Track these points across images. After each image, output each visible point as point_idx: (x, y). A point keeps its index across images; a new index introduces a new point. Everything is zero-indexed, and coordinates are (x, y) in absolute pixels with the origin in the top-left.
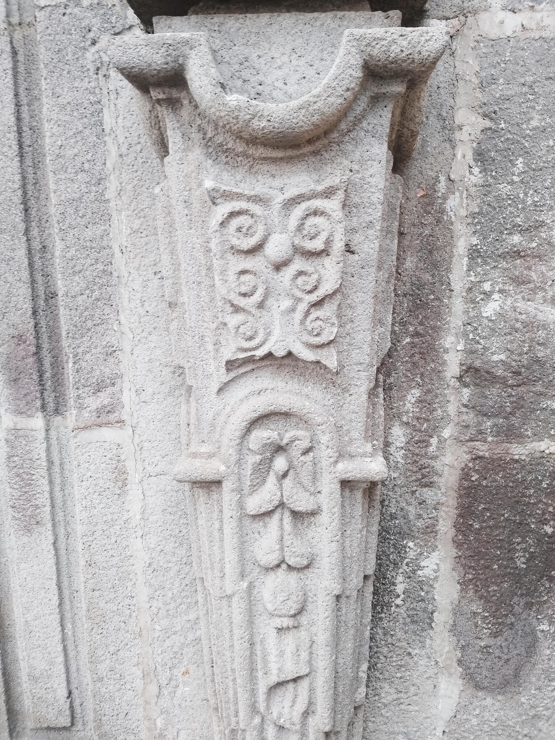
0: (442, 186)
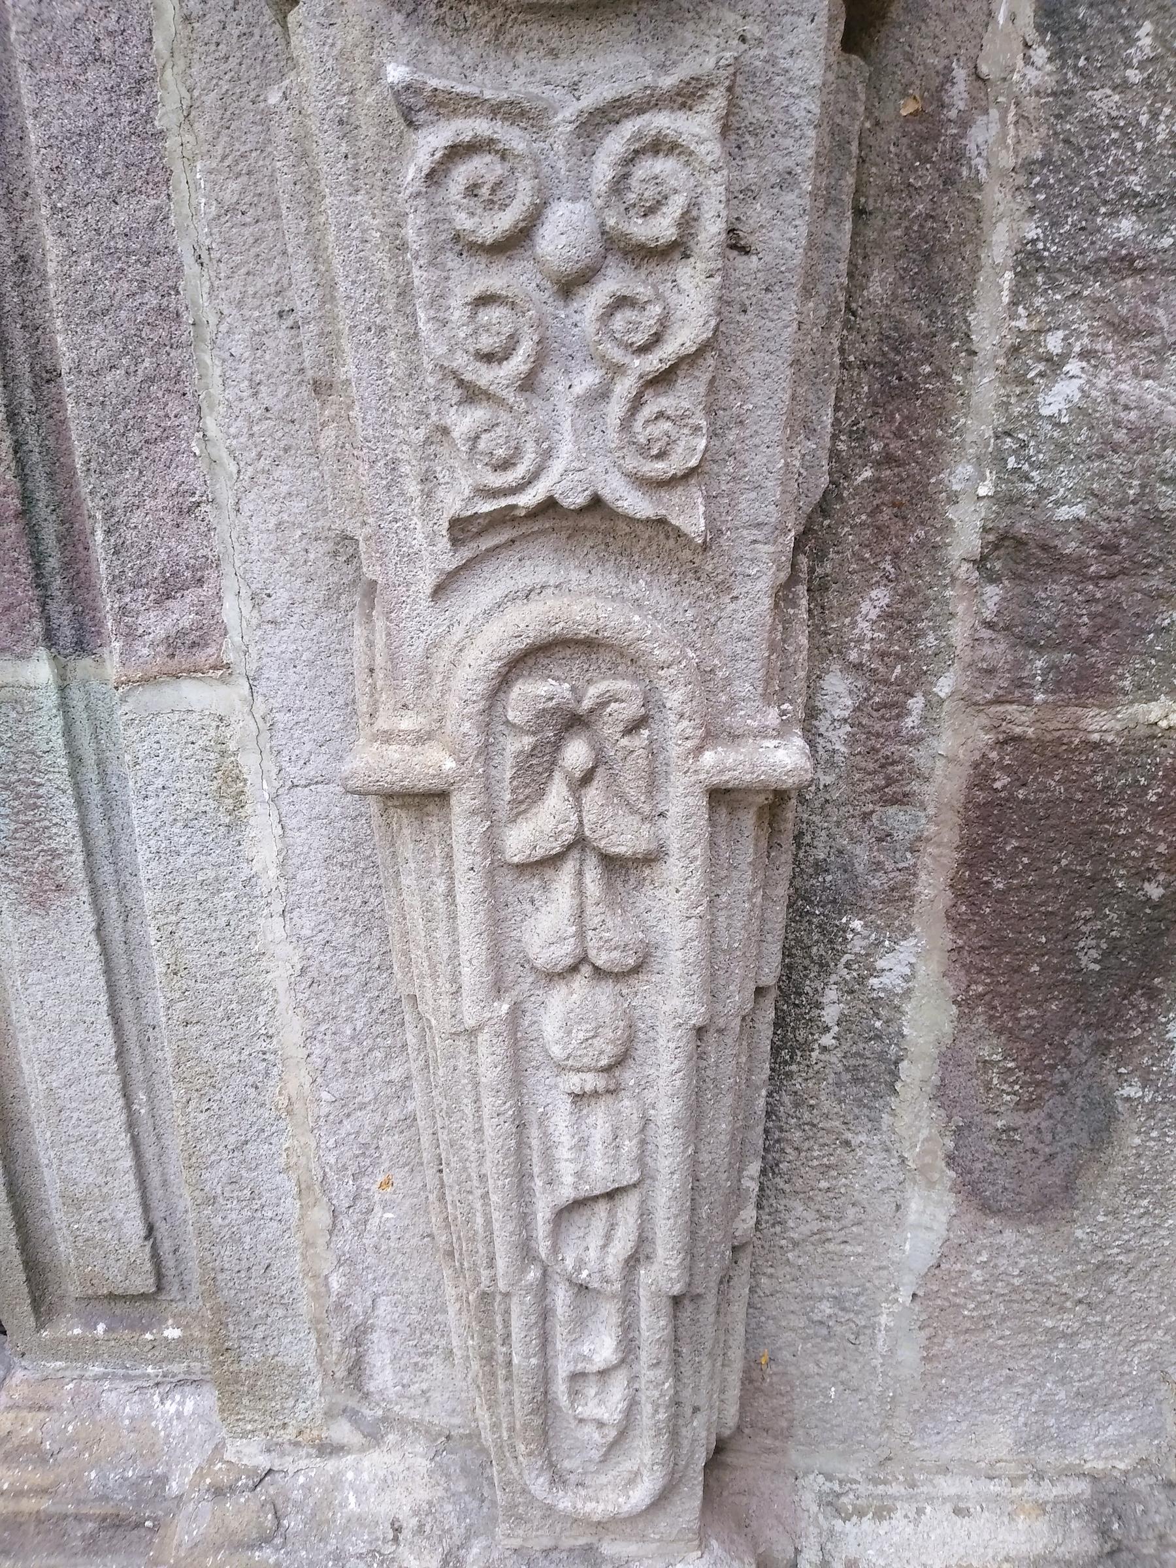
0: (959, 92)
